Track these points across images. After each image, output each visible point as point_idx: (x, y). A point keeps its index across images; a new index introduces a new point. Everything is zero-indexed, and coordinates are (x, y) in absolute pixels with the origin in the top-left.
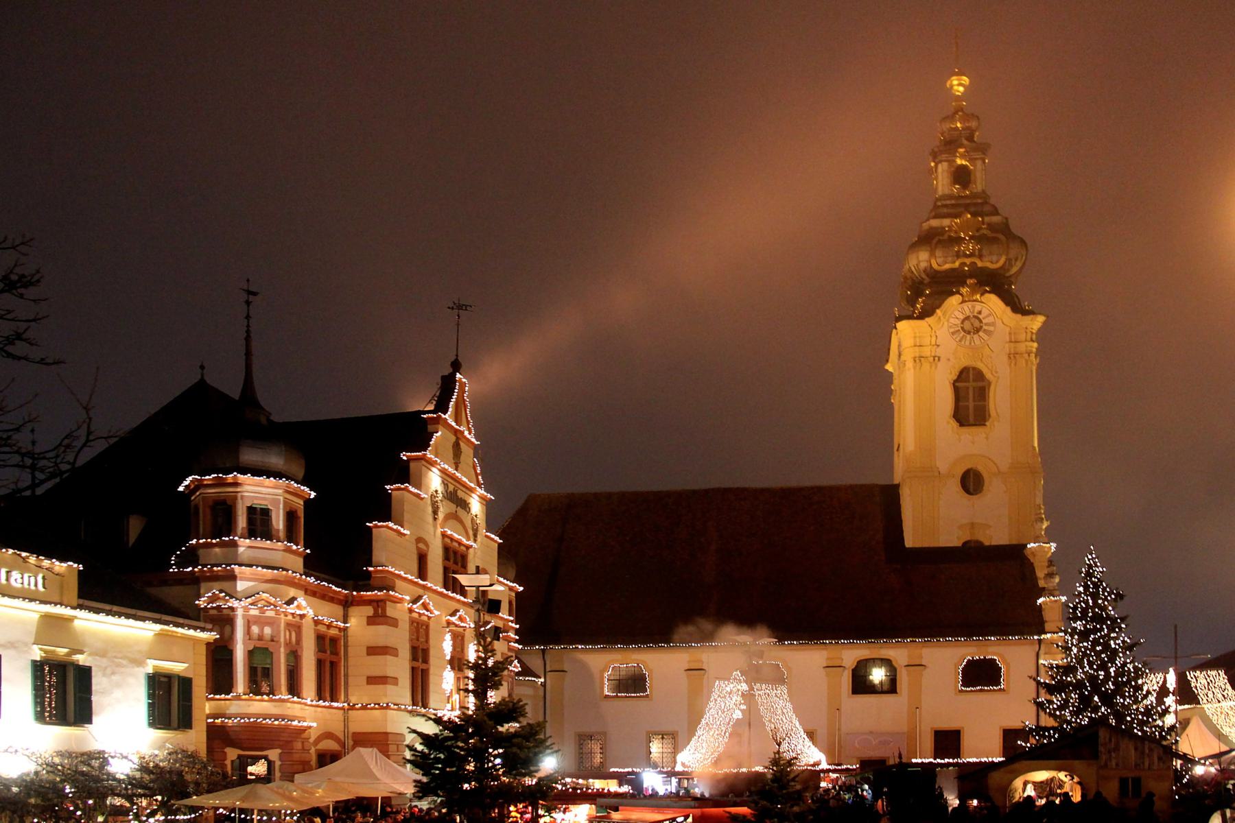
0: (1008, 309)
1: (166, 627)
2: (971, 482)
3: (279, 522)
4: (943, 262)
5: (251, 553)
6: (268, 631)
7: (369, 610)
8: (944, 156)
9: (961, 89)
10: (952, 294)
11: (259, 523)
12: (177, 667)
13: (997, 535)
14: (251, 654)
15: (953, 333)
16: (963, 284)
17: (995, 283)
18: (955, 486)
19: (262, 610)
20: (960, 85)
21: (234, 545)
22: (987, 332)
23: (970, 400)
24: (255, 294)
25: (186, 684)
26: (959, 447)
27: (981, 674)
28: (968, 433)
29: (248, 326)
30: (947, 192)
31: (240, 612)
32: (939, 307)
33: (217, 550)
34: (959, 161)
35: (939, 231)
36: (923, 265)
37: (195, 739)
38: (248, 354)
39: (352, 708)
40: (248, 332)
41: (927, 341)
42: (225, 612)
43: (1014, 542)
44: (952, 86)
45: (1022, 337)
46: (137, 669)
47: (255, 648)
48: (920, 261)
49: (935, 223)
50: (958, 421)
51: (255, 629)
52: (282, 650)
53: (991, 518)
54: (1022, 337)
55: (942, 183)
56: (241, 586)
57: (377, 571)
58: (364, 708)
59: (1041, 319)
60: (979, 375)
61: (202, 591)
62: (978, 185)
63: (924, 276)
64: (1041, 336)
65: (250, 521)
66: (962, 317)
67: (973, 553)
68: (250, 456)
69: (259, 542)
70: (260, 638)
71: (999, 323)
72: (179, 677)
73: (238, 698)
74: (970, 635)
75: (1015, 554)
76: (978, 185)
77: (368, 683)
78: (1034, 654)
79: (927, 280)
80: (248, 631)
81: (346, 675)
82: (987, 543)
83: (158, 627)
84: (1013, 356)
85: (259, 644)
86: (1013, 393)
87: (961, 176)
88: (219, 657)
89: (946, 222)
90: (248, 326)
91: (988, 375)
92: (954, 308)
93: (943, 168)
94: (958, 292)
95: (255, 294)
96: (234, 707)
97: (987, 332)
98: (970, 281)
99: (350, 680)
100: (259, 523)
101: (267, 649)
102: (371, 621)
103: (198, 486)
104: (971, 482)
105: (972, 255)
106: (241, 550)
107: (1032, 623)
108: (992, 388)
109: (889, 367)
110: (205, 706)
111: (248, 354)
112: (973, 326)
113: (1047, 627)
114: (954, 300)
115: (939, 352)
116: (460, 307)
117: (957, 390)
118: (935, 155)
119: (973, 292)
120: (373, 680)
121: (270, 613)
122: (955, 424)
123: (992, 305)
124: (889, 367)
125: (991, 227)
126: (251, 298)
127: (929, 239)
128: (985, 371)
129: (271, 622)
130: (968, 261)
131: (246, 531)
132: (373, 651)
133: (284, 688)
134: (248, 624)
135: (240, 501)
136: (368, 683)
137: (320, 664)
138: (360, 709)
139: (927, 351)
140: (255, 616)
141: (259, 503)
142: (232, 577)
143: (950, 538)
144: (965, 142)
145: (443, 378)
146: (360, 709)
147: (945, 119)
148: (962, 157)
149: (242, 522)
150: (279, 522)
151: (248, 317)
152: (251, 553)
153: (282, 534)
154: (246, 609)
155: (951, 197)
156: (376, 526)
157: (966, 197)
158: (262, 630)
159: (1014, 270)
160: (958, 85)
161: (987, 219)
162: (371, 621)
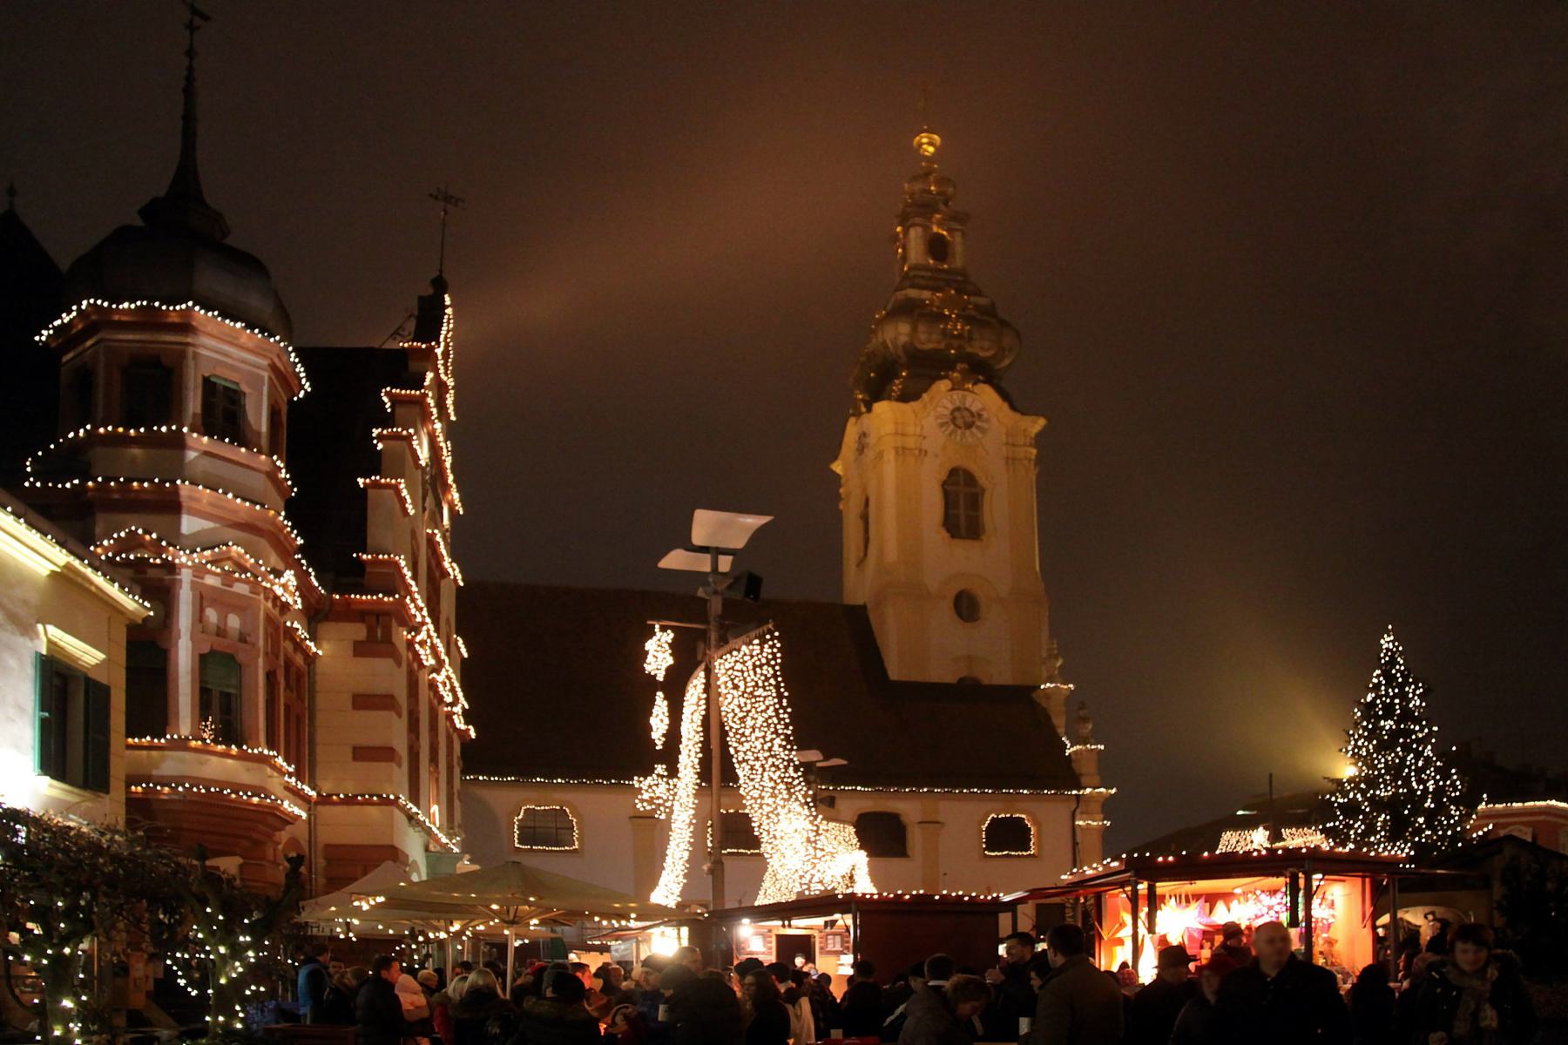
0: (1005, 406)
1: (76, 563)
2: (966, 606)
3: (259, 418)
4: (928, 340)
5: (207, 465)
6: (234, 622)
7: (359, 631)
8: (917, 220)
9: (931, 149)
10: (942, 378)
11: (224, 414)
12: (87, 655)
13: (999, 673)
14: (205, 662)
15: (942, 425)
16: (953, 369)
17: (981, 371)
18: (946, 607)
19: (227, 577)
20: (930, 144)
21: (178, 442)
22: (983, 430)
23: (962, 506)
24: (206, 18)
25: (96, 692)
26: (951, 562)
27: (1008, 835)
28: (961, 548)
29: (190, 69)
30: (921, 261)
31: (186, 576)
32: (925, 390)
33: (136, 451)
34: (935, 229)
35: (919, 303)
36: (903, 339)
37: (111, 808)
38: (189, 119)
39: (325, 800)
40: (190, 79)
41: (911, 429)
42: (151, 573)
43: (1019, 682)
44: (921, 144)
45: (1021, 441)
46: (21, 640)
47: (213, 652)
48: (898, 334)
49: (913, 293)
50: (948, 530)
51: (212, 615)
52: (261, 661)
53: (988, 651)
54: (1021, 441)
55: (916, 248)
56: (189, 525)
57: (375, 562)
58: (350, 801)
59: (1042, 422)
60: (970, 479)
61: (98, 530)
62: (958, 261)
63: (901, 352)
64: (1040, 440)
65: (207, 405)
66: (951, 407)
67: (969, 691)
68: (209, 278)
69: (225, 448)
70: (221, 632)
71: (994, 420)
72: (88, 680)
73: (182, 745)
74: (997, 787)
75: (1022, 696)
76: (958, 261)
77: (355, 758)
78: (1068, 815)
79: (904, 360)
80: (199, 617)
81: (312, 742)
82: (986, 682)
83: (62, 557)
84: (1011, 461)
85: (222, 645)
86: (1009, 500)
87: (937, 247)
88: (146, 650)
89: (926, 294)
90: (190, 69)
91: (982, 480)
92: (942, 397)
93: (915, 234)
94: (946, 377)
95: (206, 18)
96: (171, 764)
97: (983, 430)
98: (959, 366)
99: (319, 750)
100: (224, 414)
101: (232, 657)
102: (360, 649)
103: (94, 323)
104: (966, 606)
105: (960, 336)
106: (191, 455)
107: (1065, 776)
108: (987, 496)
109: (837, 467)
110: (127, 751)
111: (189, 119)
112: (964, 420)
113: (1084, 780)
114: (943, 386)
115: (925, 445)
116: (448, 199)
117: (946, 494)
118: (904, 220)
119: (965, 380)
120: (363, 753)
121: (241, 589)
122: (946, 535)
123: (984, 398)
124: (837, 467)
125: (977, 307)
126: (198, 21)
127: (908, 310)
128: (978, 474)
129: (241, 606)
130: (955, 343)
131: (199, 421)
132: (365, 701)
133: (262, 737)
134: (203, 598)
135: (191, 363)
136: (355, 758)
137: (267, 702)
138: (342, 802)
139: (911, 442)
140: (213, 588)
141: (226, 376)
142: (171, 506)
143: (942, 672)
144: (942, 207)
145: (422, 299)
146: (342, 802)
147: (914, 179)
148: (940, 225)
149: (194, 403)
150: (259, 418)
151: (190, 53)
152: (207, 465)
153: (264, 442)
154: (199, 570)
155: (927, 268)
156: (376, 485)
157: (944, 271)
158: (223, 618)
159: (1006, 362)
160: (928, 144)
161: (973, 299)
162: (360, 649)
